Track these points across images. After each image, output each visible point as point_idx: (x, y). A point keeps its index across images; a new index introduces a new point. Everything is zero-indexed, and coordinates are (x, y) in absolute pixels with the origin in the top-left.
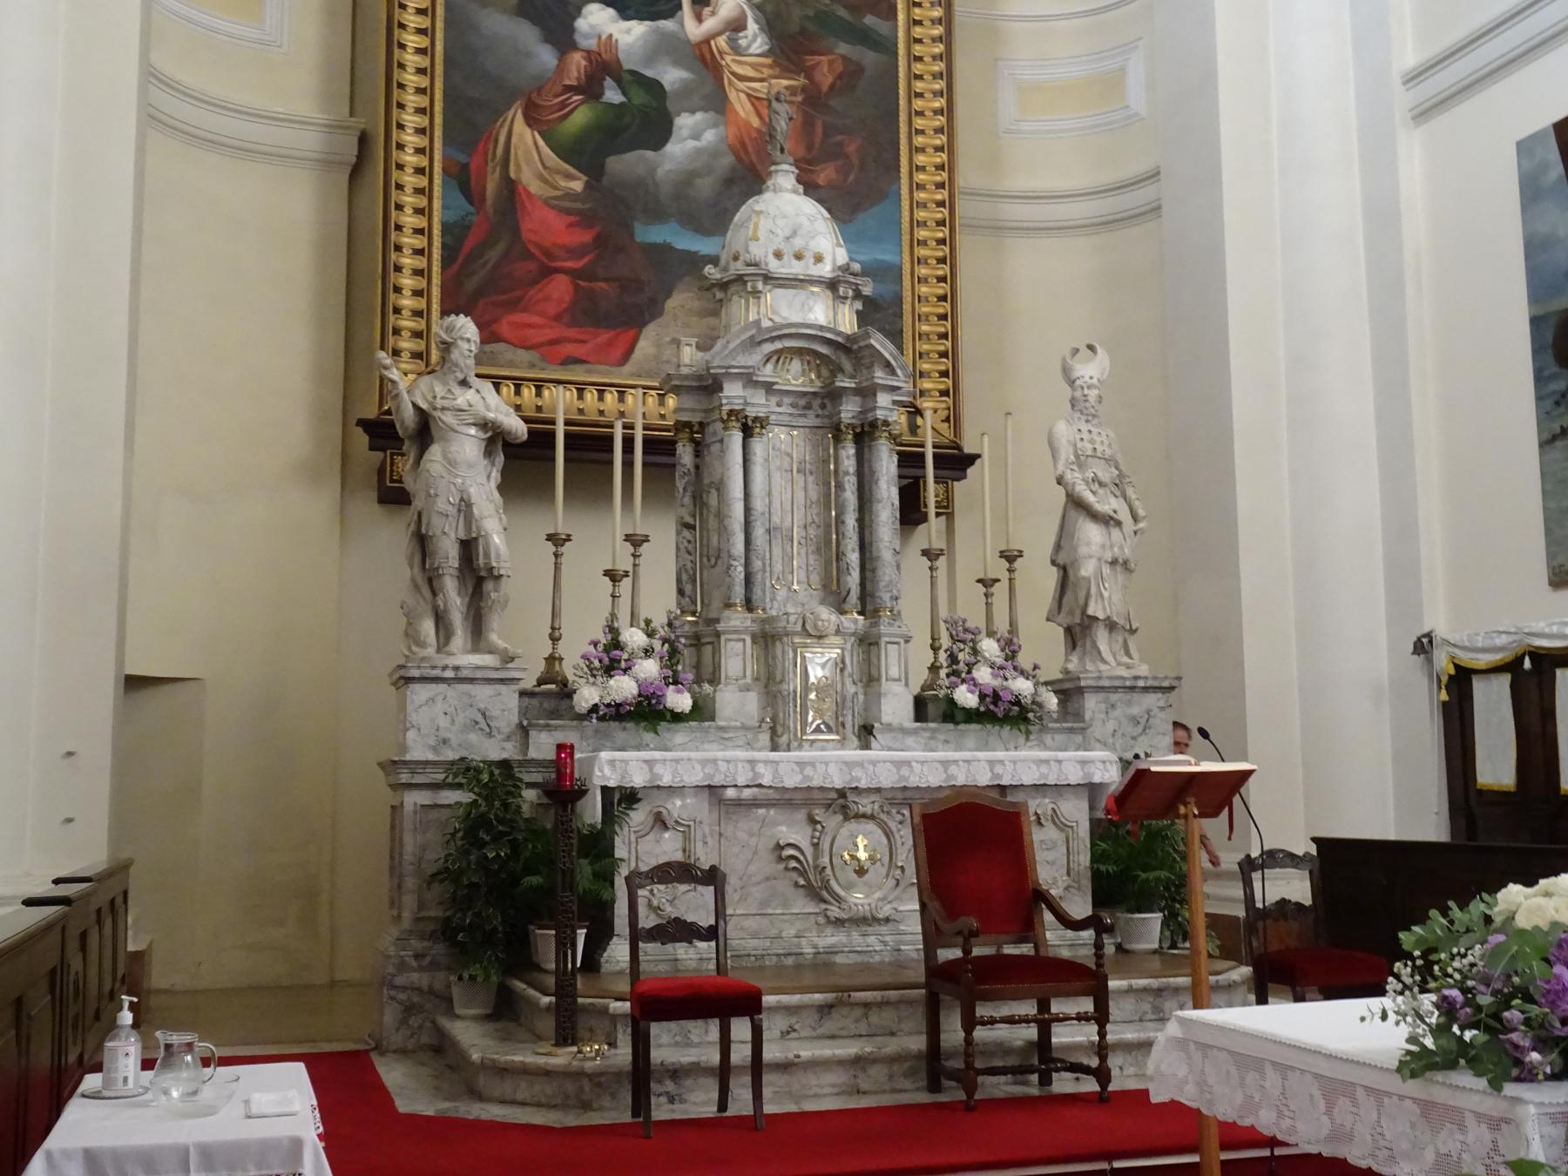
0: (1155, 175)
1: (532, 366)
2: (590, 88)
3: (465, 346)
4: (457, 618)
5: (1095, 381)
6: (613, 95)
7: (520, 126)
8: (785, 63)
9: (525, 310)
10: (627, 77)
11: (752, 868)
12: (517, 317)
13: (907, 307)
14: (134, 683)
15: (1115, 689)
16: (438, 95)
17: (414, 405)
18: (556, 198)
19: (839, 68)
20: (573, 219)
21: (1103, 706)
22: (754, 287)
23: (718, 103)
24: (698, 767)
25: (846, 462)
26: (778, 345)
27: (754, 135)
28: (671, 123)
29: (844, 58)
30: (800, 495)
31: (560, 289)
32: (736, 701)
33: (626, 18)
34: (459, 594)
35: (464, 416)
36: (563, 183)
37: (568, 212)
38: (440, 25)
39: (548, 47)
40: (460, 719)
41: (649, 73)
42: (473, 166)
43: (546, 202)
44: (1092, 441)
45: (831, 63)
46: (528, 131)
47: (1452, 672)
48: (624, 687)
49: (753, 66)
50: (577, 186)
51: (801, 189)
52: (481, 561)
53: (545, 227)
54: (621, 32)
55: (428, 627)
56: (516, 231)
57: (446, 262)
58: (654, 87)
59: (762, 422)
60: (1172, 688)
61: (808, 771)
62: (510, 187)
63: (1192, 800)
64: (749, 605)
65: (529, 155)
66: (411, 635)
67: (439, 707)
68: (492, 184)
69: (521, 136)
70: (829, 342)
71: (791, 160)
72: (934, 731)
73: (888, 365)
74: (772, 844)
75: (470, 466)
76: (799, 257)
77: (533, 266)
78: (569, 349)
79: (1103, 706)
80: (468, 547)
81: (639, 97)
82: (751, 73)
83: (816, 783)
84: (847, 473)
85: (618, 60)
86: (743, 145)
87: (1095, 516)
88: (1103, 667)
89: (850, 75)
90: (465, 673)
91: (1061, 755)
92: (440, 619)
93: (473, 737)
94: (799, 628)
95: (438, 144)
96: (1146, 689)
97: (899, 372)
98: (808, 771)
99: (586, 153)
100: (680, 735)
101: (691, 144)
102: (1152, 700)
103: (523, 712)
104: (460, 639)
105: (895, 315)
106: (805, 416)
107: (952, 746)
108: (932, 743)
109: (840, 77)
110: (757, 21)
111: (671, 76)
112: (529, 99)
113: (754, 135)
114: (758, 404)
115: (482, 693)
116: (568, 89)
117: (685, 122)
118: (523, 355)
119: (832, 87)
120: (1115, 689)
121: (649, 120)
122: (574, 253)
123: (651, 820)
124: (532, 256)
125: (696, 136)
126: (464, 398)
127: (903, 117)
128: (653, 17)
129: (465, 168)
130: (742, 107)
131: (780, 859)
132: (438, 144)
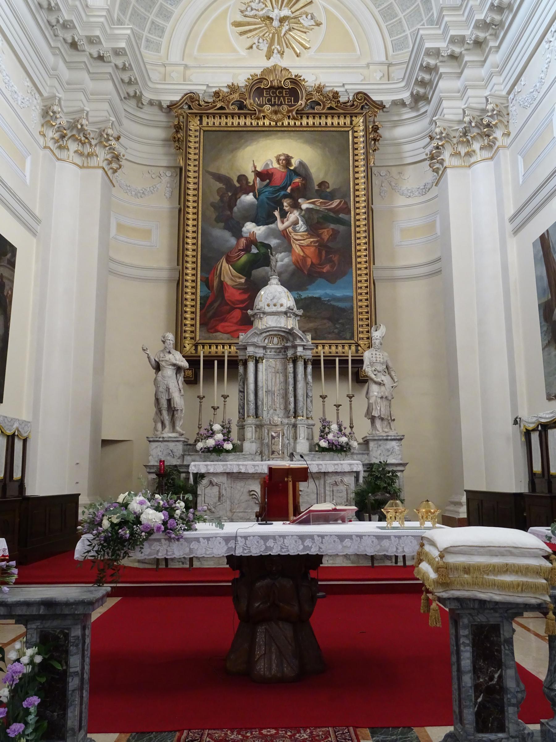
0: (439, 259)
1: (228, 339)
2: (247, 249)
4: (167, 423)
5: (378, 337)
6: (254, 250)
7: (225, 264)
8: (312, 233)
9: (225, 322)
10: (259, 244)
11: (242, 498)
12: (223, 324)
13: (355, 310)
14: (105, 443)
15: (380, 440)
16: (199, 257)
18: (236, 285)
19: (331, 232)
20: (241, 291)
21: (376, 445)
23: (289, 249)
24: (222, 467)
26: (268, 334)
29: (333, 229)
30: (278, 380)
32: (249, 446)
34: (168, 415)
36: (238, 280)
37: (239, 289)
40: (165, 453)
41: (266, 242)
42: (210, 279)
43: (233, 287)
44: (376, 357)
47: (525, 431)
48: (211, 442)
49: (301, 236)
50: (243, 281)
51: (279, 283)
52: (172, 405)
53: (233, 295)
55: (159, 425)
56: (223, 297)
58: (268, 246)
59: (262, 358)
60: (401, 439)
61: (257, 468)
62: (222, 284)
63: (290, 476)
64: (257, 416)
65: (228, 273)
66: (155, 429)
67: (159, 449)
69: (225, 267)
70: (284, 332)
71: (277, 274)
72: (314, 454)
73: (301, 338)
74: (248, 490)
76: (275, 305)
77: (228, 307)
79: (376, 445)
80: (169, 401)
81: (263, 250)
82: (300, 238)
83: (259, 472)
84: (290, 373)
86: (298, 262)
87: (376, 383)
88: (377, 432)
89: (335, 233)
90: (166, 439)
91: (342, 462)
92: (163, 423)
93: (169, 458)
94: (269, 423)
95: (199, 272)
96: (392, 440)
97: (304, 340)
98: (257, 468)
100: (231, 456)
102: (394, 443)
103: (184, 451)
104: (167, 429)
107: (321, 459)
108: (314, 458)
109: (331, 235)
110: (302, 221)
111: (273, 242)
113: (301, 258)
114: (260, 353)
115: (171, 445)
116: (240, 250)
119: (328, 240)
120: (380, 440)
122: (242, 302)
123: (209, 483)
124: (228, 304)
125: (282, 261)
126: (169, 357)
127: (353, 245)
128: (267, 224)
129: (207, 278)
130: (297, 249)
131: (250, 495)
132: (199, 272)
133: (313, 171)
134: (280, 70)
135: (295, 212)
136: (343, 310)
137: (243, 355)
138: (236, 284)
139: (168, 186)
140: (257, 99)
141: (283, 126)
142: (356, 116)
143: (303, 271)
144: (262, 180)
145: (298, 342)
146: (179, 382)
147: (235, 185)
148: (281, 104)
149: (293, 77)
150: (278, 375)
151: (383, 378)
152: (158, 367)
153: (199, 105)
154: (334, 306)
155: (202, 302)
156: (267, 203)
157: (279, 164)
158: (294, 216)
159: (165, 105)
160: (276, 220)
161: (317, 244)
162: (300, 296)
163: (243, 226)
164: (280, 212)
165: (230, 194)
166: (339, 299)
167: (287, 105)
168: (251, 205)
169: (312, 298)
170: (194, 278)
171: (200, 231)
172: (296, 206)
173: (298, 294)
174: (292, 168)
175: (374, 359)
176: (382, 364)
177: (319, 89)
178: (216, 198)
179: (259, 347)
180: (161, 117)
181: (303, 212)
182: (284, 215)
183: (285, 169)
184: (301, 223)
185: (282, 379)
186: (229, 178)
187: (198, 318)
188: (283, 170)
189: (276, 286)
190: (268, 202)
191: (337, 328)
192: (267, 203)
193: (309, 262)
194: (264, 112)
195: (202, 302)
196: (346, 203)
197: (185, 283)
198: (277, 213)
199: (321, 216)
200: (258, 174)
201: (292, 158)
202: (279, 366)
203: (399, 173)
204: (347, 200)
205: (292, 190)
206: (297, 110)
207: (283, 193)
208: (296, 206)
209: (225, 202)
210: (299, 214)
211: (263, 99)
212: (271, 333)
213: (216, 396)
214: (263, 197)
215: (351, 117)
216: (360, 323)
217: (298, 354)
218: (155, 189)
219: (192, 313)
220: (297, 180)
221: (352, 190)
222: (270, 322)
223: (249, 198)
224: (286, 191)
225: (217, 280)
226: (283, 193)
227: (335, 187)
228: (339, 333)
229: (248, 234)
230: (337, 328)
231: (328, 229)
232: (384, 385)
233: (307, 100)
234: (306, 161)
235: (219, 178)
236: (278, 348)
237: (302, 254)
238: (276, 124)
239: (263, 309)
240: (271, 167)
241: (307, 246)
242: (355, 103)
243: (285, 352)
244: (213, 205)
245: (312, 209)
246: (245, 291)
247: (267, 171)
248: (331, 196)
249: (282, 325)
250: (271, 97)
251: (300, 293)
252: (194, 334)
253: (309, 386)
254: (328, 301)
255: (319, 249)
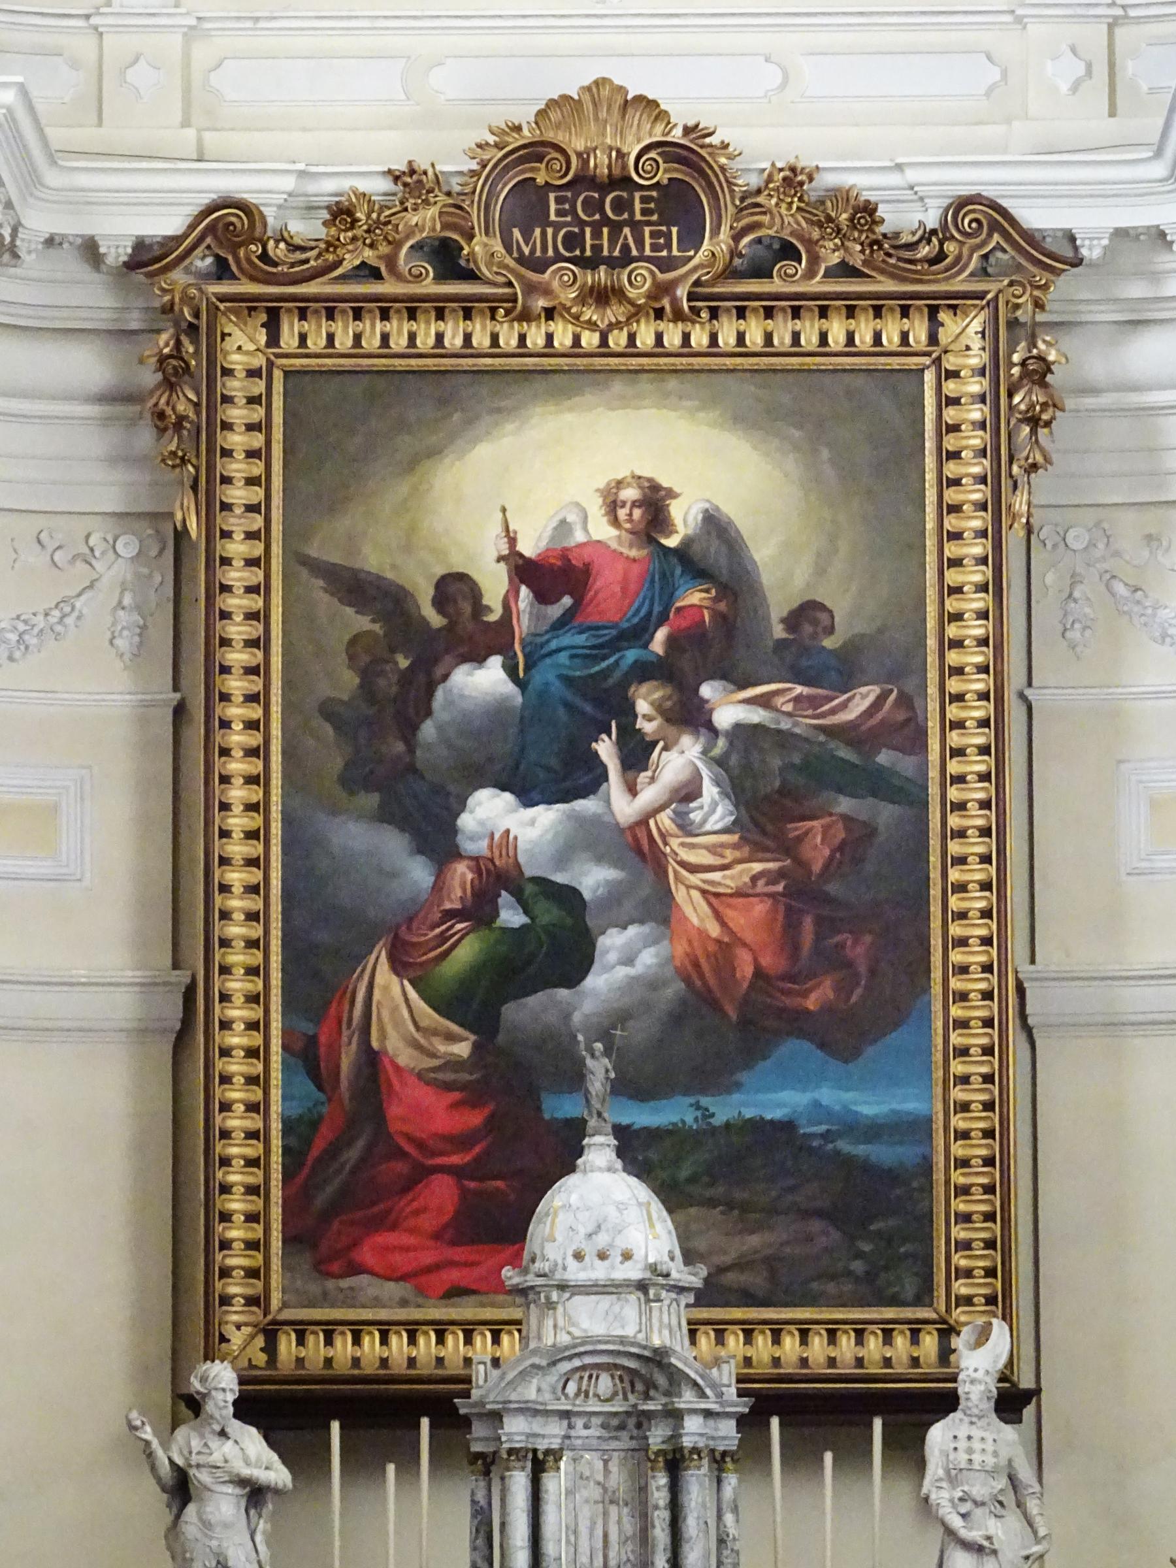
1: (404, 1303)
2: (479, 910)
3: (219, 1396)
5: (980, 1375)
6: (511, 916)
7: (385, 975)
8: (757, 837)
9: (394, 1227)
10: (529, 889)
12: (391, 1238)
13: (939, 1176)
17: (170, 1459)
20: (456, 1095)
22: (548, 1298)
23: (659, 909)
25: (656, 1494)
26: (577, 1363)
27: (712, 948)
28: (592, 945)
29: (847, 819)
31: (441, 1196)
33: (528, 803)
35: (219, 1473)
36: (442, 1048)
37: (448, 1087)
38: (276, 850)
39: (421, 859)
41: (560, 878)
42: (323, 1039)
43: (420, 1076)
44: (970, 1451)
45: (826, 829)
46: (395, 979)
49: (712, 849)
50: (462, 1049)
51: (619, 1164)
54: (523, 824)
56: (379, 1117)
57: (288, 1176)
58: (569, 897)
59: (557, 1455)
62: (372, 1061)
65: (397, 1012)
68: (347, 1061)
69: (386, 989)
70: (639, 1357)
73: (696, 1384)
75: (226, 1526)
76: (602, 1256)
77: (401, 1167)
78: (454, 1276)
81: (549, 913)
82: (706, 858)
84: (656, 1507)
85: (518, 865)
86: (696, 965)
87: (967, 1546)
89: (857, 840)
97: (708, 1391)
99: (473, 1003)
101: (622, 972)
105: (921, 1190)
106: (616, 1438)
109: (841, 848)
111: (592, 879)
112: (396, 936)
113: (712, 948)
114: (551, 1434)
116: (449, 915)
117: (612, 942)
118: (393, 1289)
121: (562, 946)
122: (462, 1142)
124: (402, 1154)
125: (629, 961)
126: (222, 1451)
129: (312, 1041)
130: (693, 909)
133: (764, 553)
134: (620, 101)
135: (686, 740)
136: (892, 1176)
137: (486, 1439)
138: (436, 1063)
139: (127, 600)
140: (517, 233)
141: (632, 349)
142: (954, 308)
143: (715, 1005)
144: (542, 597)
145: (687, 1399)
146: (259, 1538)
147: (424, 621)
148: (626, 259)
149: (677, 135)
150: (613, 1510)
151: (994, 1527)
152: (181, 1489)
153: (264, 257)
154: (847, 1163)
155: (293, 1142)
156: (567, 705)
157: (615, 522)
158: (680, 759)
159: (117, 252)
160: (605, 777)
161: (780, 888)
162: (708, 1115)
163: (462, 806)
164: (621, 744)
165: (403, 663)
166: (874, 1131)
167: (649, 260)
168: (497, 712)
169: (757, 1126)
170: (257, 1040)
171: (276, 828)
172: (690, 715)
173: (698, 1107)
174: (672, 542)
175: (963, 1457)
176: (992, 1473)
177: (793, 180)
178: (347, 682)
179: (547, 1413)
180: (94, 299)
181: (721, 743)
182: (637, 755)
183: (640, 548)
184: (710, 791)
185: (630, 1526)
186: (402, 588)
187: (276, 1212)
188: (633, 553)
189: (607, 1177)
190: (569, 696)
191: (859, 1255)
192: (567, 705)
193: (745, 969)
194: (547, 292)
195: (293, 1142)
196: (905, 701)
197: (220, 1064)
198: (606, 749)
199: (797, 759)
200: (524, 570)
201: (671, 494)
202: (618, 1478)
203: (1149, 538)
204: (910, 686)
205: (671, 641)
206: (697, 283)
207: (631, 655)
208: (690, 715)
209: (381, 696)
210: (705, 752)
211: (544, 234)
212: (588, 1361)
213: (337, 1538)
214: (546, 675)
215: (933, 311)
216: (959, 1233)
217: (687, 1442)
218: (69, 621)
219: (252, 1190)
220: (694, 597)
221: (932, 642)
222: (591, 1320)
223: (484, 681)
224: (646, 646)
225: (354, 1046)
226: (631, 655)
227: (861, 627)
228: (870, 1277)
229: (485, 843)
230: (859, 1255)
231: (828, 820)
232: (994, 1552)
233: (737, 238)
234: (730, 510)
235: (356, 588)
236: (616, 1414)
237: (714, 930)
238: (604, 342)
239: (558, 1275)
240: (579, 537)
241: (739, 894)
242: (951, 248)
243: (639, 1426)
244: (328, 711)
245: (757, 729)
246: (472, 1096)
247: (565, 554)
248: (843, 672)
249: (630, 1331)
250: (582, 224)
251: (705, 1101)
252: (260, 1284)
253: (726, 1553)
254: (826, 1136)
255: (789, 910)
